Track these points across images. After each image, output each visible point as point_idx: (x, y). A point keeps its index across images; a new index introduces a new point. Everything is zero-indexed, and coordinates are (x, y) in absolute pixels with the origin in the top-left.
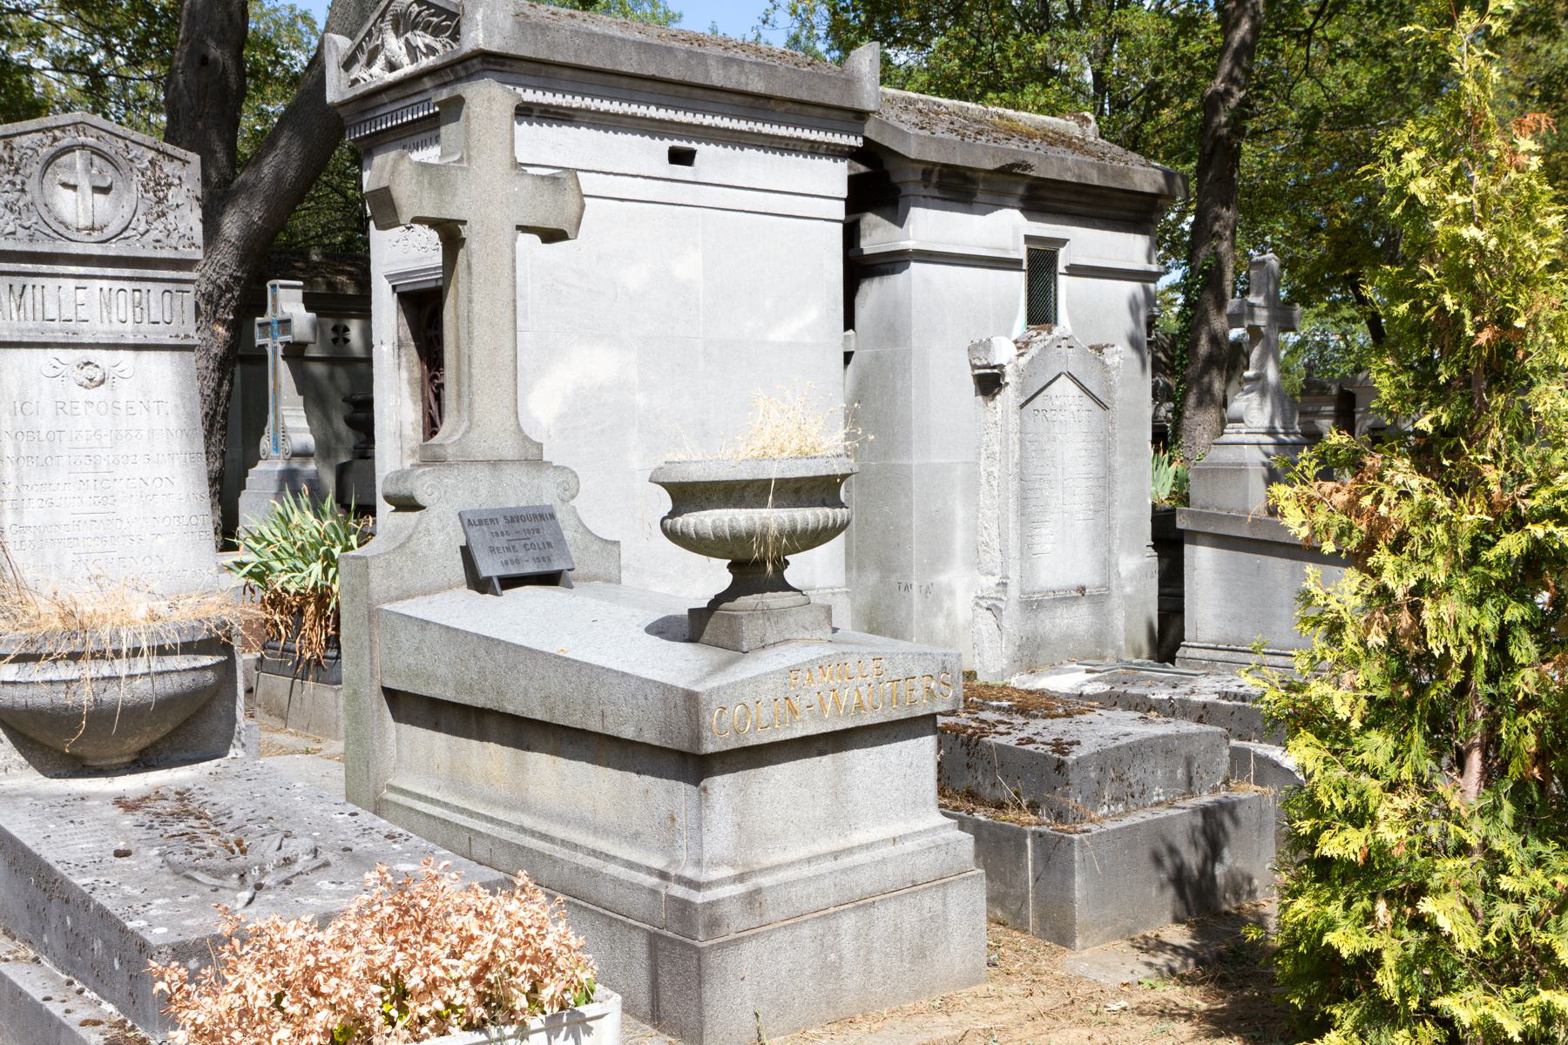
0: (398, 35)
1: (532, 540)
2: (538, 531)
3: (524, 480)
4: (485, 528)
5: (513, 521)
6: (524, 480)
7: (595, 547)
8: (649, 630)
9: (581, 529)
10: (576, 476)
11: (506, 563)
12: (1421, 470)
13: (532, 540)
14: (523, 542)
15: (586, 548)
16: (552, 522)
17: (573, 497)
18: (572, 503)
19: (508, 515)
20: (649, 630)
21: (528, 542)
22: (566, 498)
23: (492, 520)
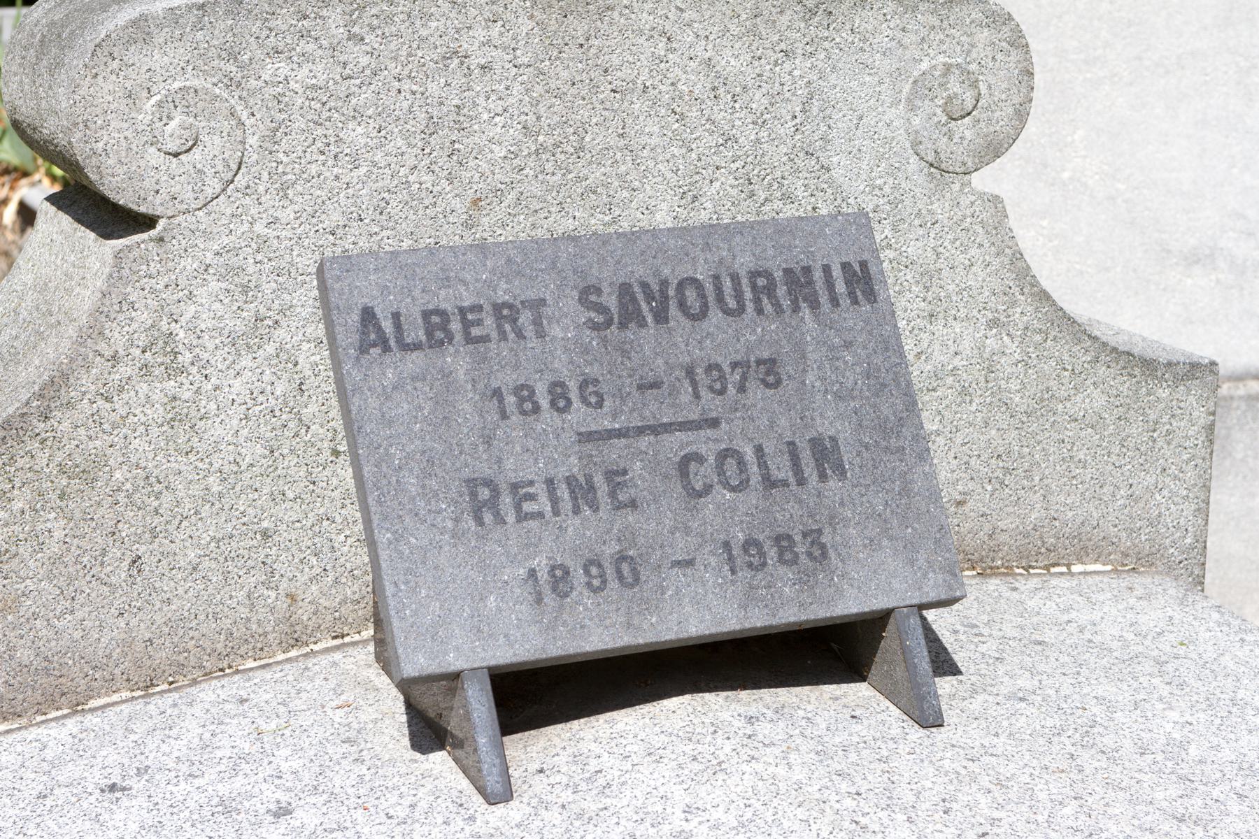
0: (421, 341)
1: (732, 433)
2: (770, 371)
3: (733, 62)
4: (457, 360)
5: (630, 316)
6: (733, 62)
7: (1092, 400)
8: (959, 672)
9: (1024, 313)
10: (1018, 42)
11: (560, 578)
12: (716, 460)
13: (732, 433)
14: (676, 444)
15: (1045, 402)
16: (852, 317)
17: (994, 150)
18: (983, 180)
19: (607, 277)
20: (959, 672)
21: (706, 444)
22: (955, 153)
23: (505, 313)
